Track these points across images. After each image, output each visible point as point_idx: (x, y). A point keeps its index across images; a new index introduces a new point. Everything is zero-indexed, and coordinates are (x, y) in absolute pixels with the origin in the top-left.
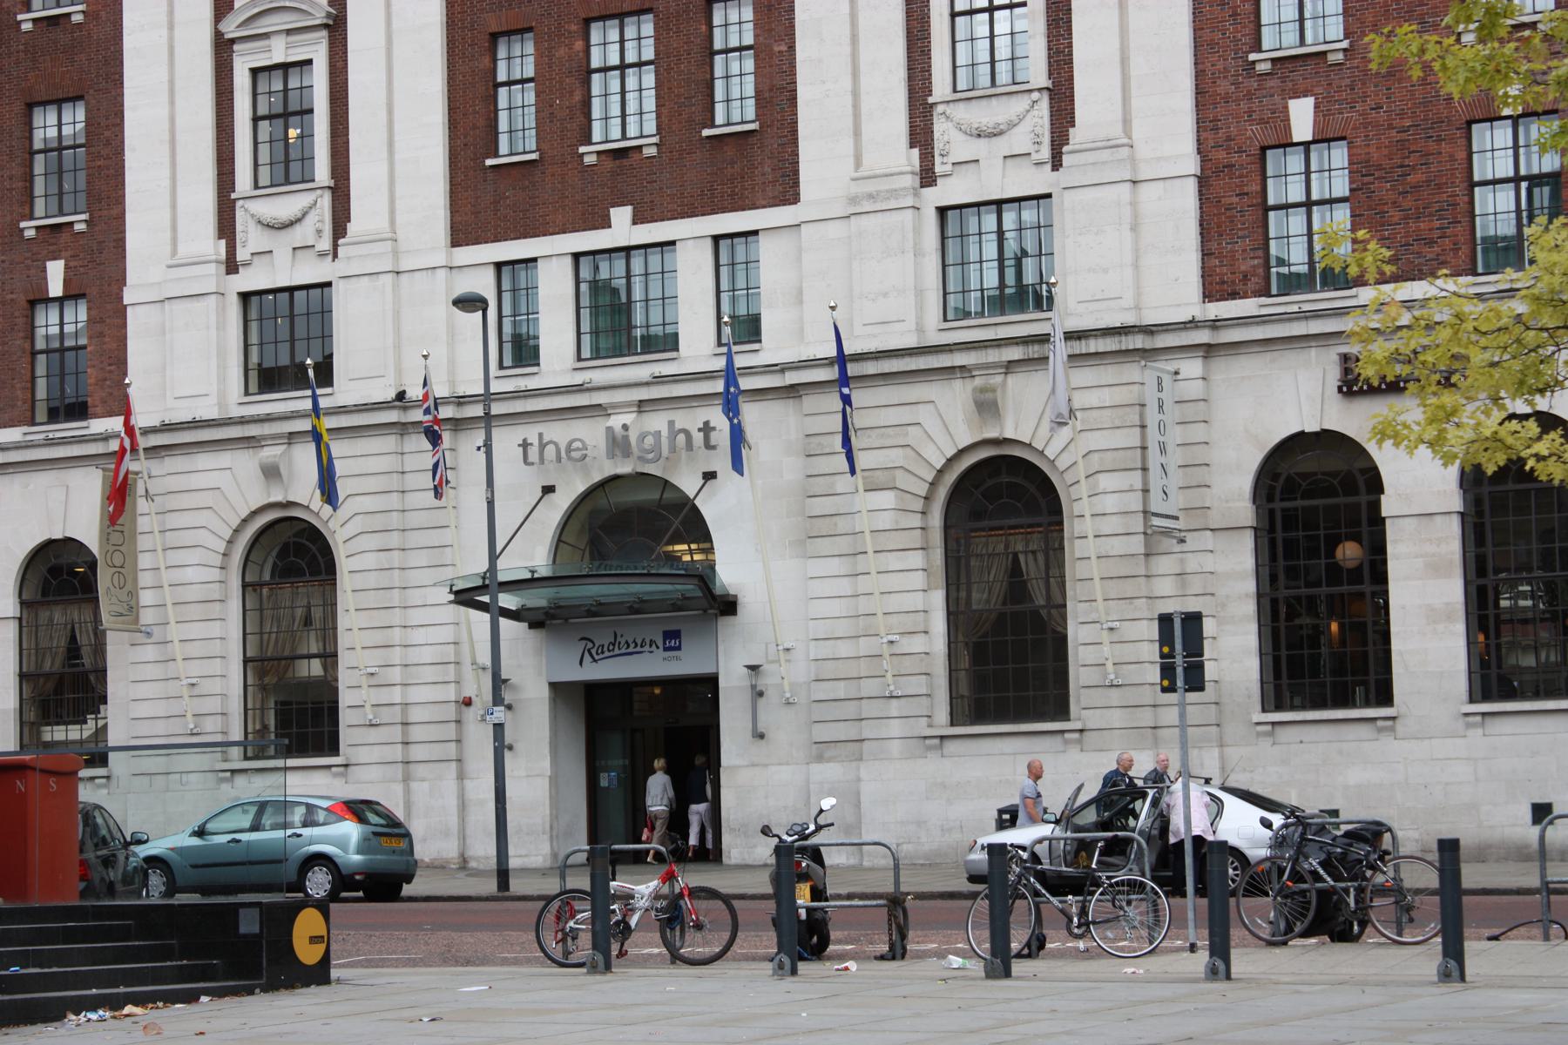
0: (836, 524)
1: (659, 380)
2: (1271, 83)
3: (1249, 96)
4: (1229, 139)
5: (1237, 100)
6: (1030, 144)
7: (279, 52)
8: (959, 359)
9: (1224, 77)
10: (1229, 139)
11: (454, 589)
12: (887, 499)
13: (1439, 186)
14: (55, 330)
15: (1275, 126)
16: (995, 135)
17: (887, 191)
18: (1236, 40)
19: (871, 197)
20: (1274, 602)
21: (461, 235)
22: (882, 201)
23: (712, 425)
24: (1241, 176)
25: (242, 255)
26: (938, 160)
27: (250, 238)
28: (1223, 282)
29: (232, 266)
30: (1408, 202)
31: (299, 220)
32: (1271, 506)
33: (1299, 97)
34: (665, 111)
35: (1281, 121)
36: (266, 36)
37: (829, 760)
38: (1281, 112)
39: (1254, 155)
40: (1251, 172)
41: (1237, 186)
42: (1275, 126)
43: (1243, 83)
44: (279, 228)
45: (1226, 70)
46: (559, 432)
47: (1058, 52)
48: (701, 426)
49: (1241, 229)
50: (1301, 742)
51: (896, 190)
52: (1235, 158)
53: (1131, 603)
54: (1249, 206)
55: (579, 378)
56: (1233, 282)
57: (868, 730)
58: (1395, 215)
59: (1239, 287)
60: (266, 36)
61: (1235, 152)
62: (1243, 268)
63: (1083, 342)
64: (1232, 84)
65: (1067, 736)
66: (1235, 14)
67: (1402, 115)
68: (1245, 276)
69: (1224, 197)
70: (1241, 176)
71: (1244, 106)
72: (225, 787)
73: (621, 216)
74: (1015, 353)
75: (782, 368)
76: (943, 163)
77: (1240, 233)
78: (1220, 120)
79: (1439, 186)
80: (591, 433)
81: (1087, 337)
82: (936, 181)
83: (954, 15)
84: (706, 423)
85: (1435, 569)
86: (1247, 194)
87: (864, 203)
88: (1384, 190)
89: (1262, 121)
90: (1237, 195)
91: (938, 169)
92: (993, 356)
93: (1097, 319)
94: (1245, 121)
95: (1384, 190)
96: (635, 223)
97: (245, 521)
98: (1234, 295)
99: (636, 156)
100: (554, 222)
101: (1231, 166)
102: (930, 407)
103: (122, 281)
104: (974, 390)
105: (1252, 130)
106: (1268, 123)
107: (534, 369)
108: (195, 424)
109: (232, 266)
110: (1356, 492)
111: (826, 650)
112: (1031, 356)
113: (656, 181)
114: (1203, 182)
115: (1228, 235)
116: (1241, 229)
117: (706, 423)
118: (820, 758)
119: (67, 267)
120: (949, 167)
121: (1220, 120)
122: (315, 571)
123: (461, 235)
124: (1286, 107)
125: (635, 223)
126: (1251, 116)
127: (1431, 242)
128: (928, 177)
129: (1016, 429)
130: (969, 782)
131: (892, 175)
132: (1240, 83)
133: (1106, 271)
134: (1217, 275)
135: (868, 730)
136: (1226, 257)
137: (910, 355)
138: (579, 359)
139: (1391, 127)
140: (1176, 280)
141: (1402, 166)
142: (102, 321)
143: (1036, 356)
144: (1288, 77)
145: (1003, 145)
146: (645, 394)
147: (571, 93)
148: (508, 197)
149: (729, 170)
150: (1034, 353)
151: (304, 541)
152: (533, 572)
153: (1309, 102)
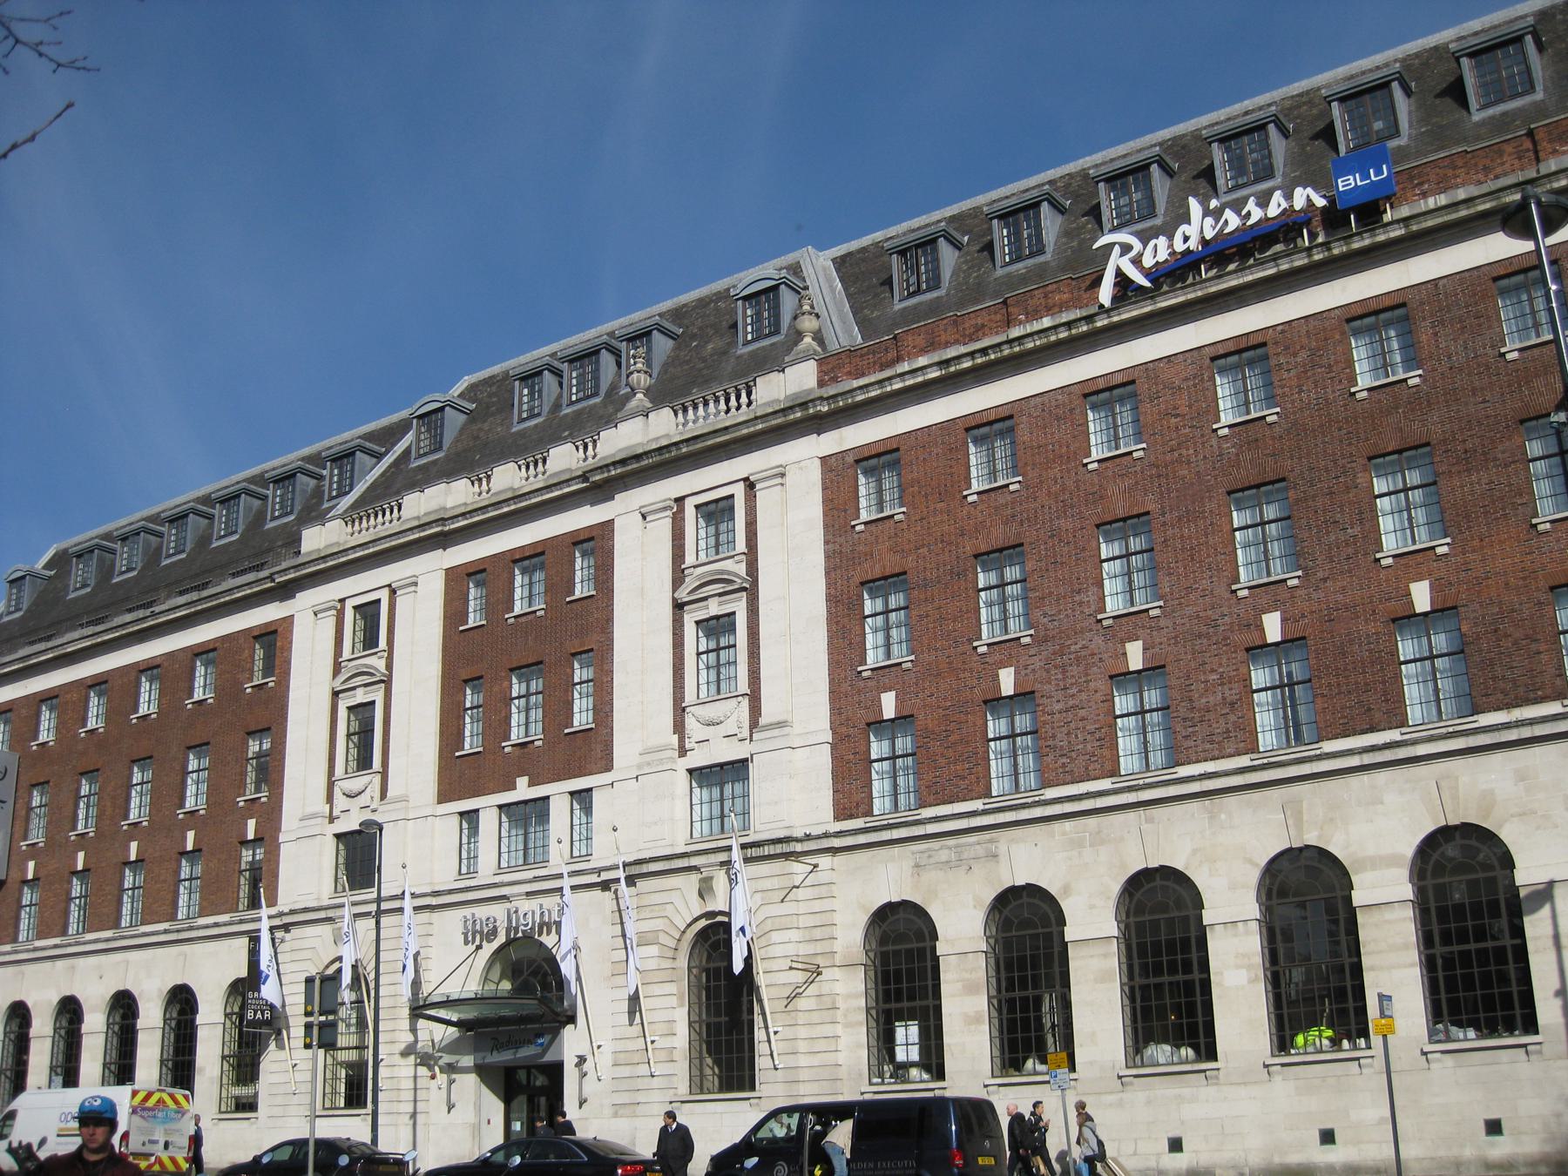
1: (536, 879)
2: (1299, 592)
4: (848, 719)
5: (852, 695)
7: (714, 608)
8: (695, 861)
12: (653, 950)
13: (967, 742)
14: (250, 859)
18: (851, 659)
20: (1132, 989)
21: (444, 797)
24: (855, 742)
26: (687, 741)
27: (340, 802)
29: (683, 752)
30: (950, 753)
31: (360, 793)
34: (547, 719)
36: (705, 599)
46: (482, 912)
47: (753, 672)
55: (497, 879)
57: (640, 1097)
58: (942, 761)
60: (705, 599)
65: (751, 1101)
66: (851, 643)
67: (945, 699)
70: (855, 742)
73: (522, 782)
75: (599, 871)
79: (967, 742)
80: (498, 912)
81: (763, 845)
83: (699, 654)
85: (970, 989)
88: (935, 747)
89: (866, 708)
91: (688, 746)
95: (935, 747)
97: (689, 925)
99: (530, 746)
101: (848, 736)
102: (678, 892)
103: (279, 829)
104: (700, 880)
108: (306, 910)
109: (332, 819)
110: (924, 941)
111: (621, 1046)
114: (834, 746)
118: (616, 1115)
119: (1284, 620)
127: (964, 778)
135: (640, 1097)
137: (874, 831)
138: (460, 874)
139: (939, 707)
141: (946, 731)
142: (270, 853)
147: (500, 712)
152: (448, 997)
153: (1139, 644)
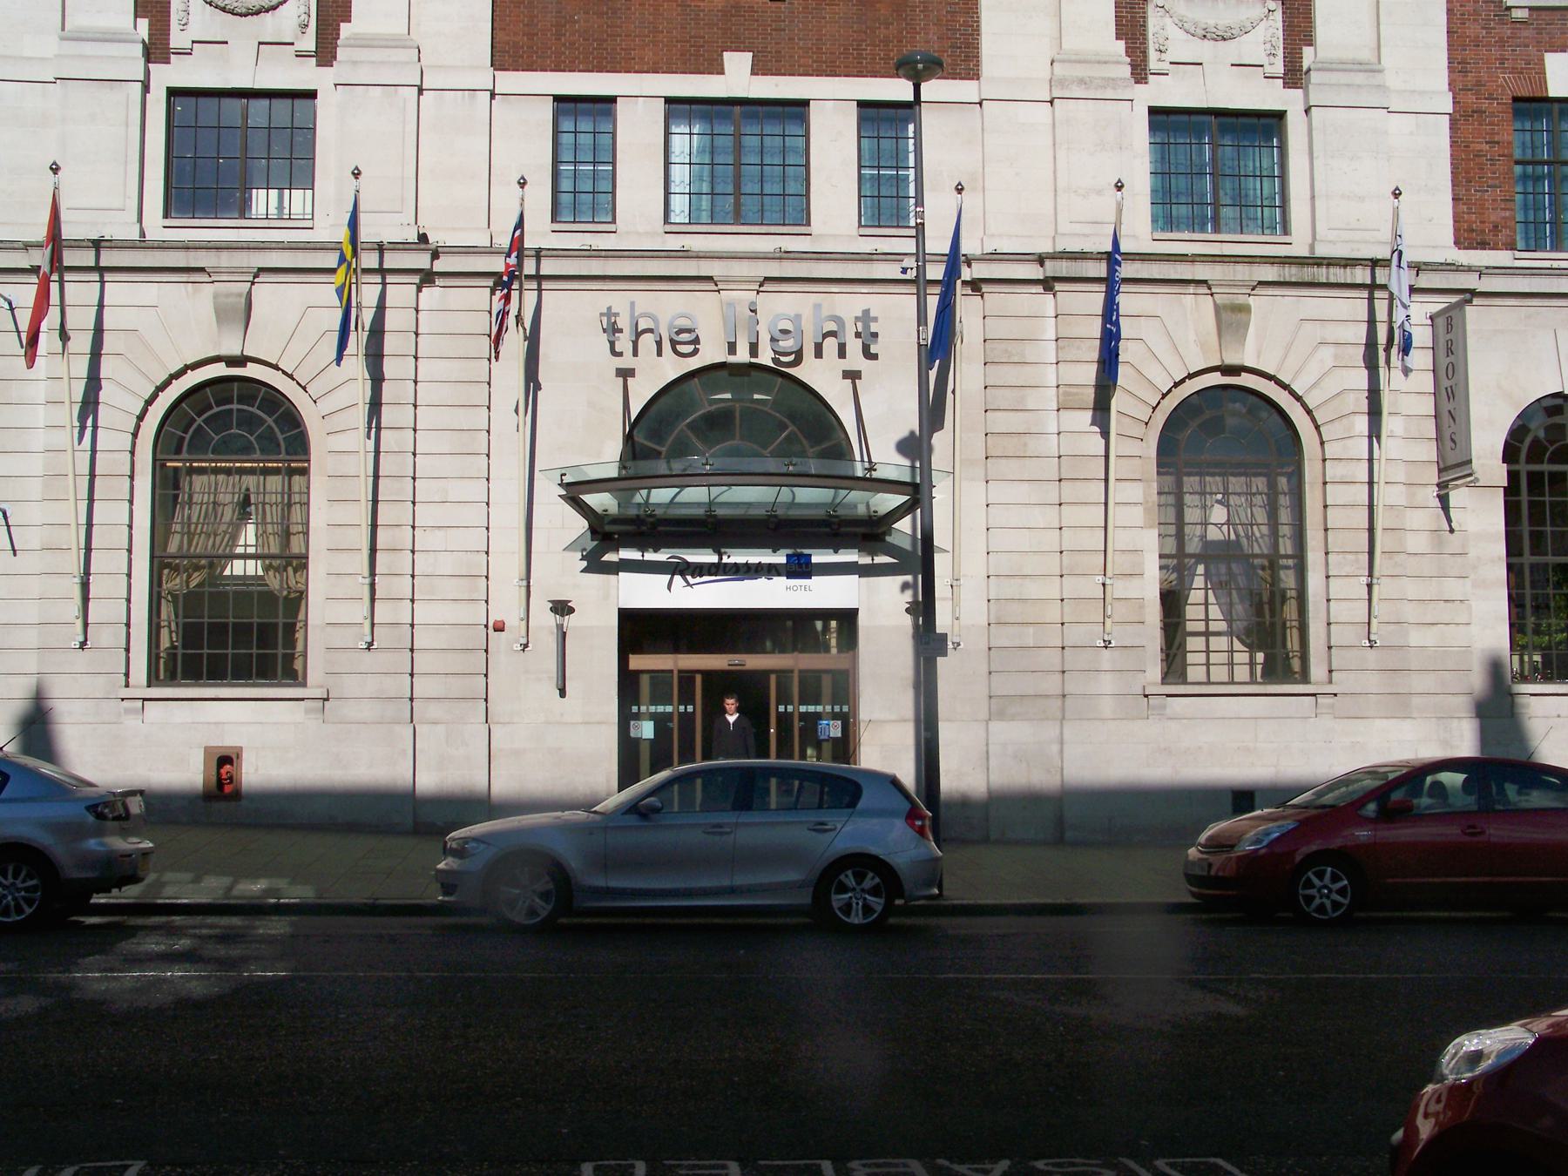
0: (1025, 445)
1: (784, 256)
2: (1527, 33)
3: (1502, 43)
4: (1479, 83)
6: (1264, 54)
9: (1474, 20)
10: (1479, 83)
11: (567, 479)
15: (1529, 78)
16: (1225, 39)
17: (1103, 79)
19: (1081, 81)
22: (1096, 89)
23: (872, 314)
25: (177, 39)
26: (1153, 55)
28: (1473, 230)
32: (1515, 467)
33: (1556, 51)
35: (1536, 73)
37: (1013, 718)
38: (1536, 64)
39: (1505, 104)
40: (1503, 120)
41: (1487, 134)
42: (1529, 78)
43: (1495, 29)
44: (241, 15)
45: (1476, 13)
48: (860, 314)
49: (1492, 178)
50: (1559, 716)
51: (1113, 79)
52: (1485, 104)
53: (1390, 558)
54: (1499, 156)
56: (1483, 231)
59: (1489, 238)
61: (1486, 99)
62: (1493, 218)
63: (1348, 270)
64: (1483, 28)
68: (1496, 227)
69: (1474, 142)
71: (1495, 52)
72: (132, 722)
74: (1269, 273)
76: (1159, 60)
77: (1490, 182)
78: (1469, 63)
82: (1146, 78)
84: (866, 312)
86: (1498, 143)
87: (1074, 87)
89: (1513, 70)
90: (1487, 143)
92: (1242, 272)
93: (1353, 250)
94: (1496, 68)
96: (754, 73)
98: (1483, 245)
100: (642, 59)
105: (1504, 78)
106: (1522, 73)
107: (611, 227)
112: (1287, 280)
113: (784, 30)
114: (1456, 123)
115: (1476, 182)
116: (1492, 178)
117: (866, 312)
120: (1165, 66)
121: (1469, 63)
122: (269, 444)
123: (506, 56)
124: (1542, 61)
125: (754, 73)
126: (1504, 64)
128: (1140, 72)
129: (1259, 357)
130: (1200, 748)
131: (1106, 63)
132: (1491, 28)
133: (1362, 199)
134: (1464, 222)
136: (1475, 204)
140: (1430, 221)
143: (1293, 280)
144: (1546, 29)
145: (1230, 51)
146: (774, 270)
148: (576, 22)
149: (882, 30)
150: (1291, 276)
151: (254, 410)
